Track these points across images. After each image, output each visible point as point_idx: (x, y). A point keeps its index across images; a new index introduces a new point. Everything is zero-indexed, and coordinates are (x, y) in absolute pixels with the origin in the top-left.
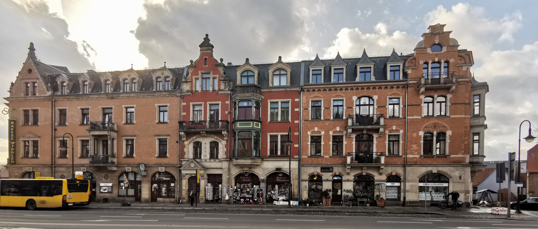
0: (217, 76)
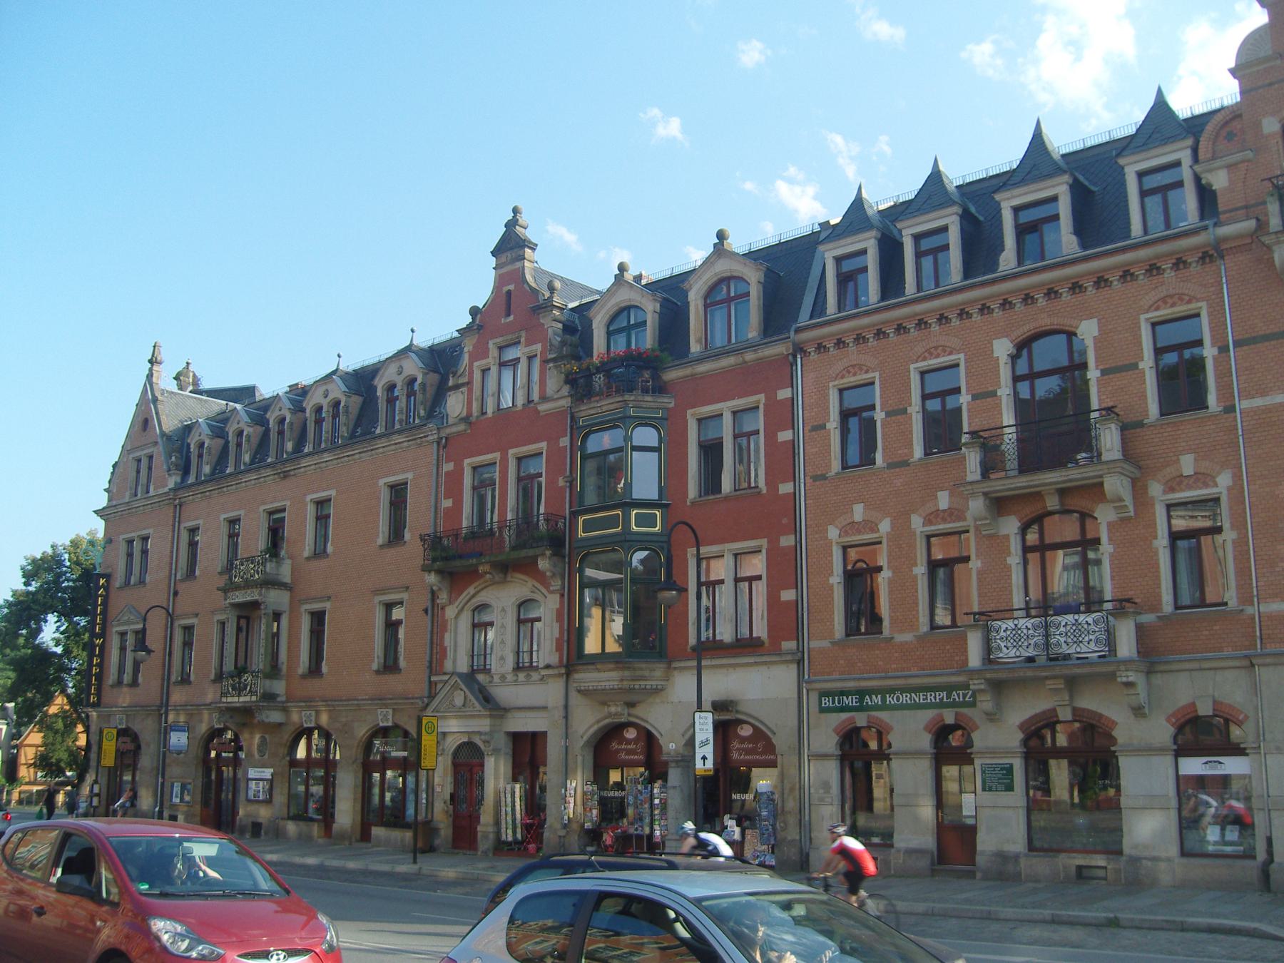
0: (538, 347)
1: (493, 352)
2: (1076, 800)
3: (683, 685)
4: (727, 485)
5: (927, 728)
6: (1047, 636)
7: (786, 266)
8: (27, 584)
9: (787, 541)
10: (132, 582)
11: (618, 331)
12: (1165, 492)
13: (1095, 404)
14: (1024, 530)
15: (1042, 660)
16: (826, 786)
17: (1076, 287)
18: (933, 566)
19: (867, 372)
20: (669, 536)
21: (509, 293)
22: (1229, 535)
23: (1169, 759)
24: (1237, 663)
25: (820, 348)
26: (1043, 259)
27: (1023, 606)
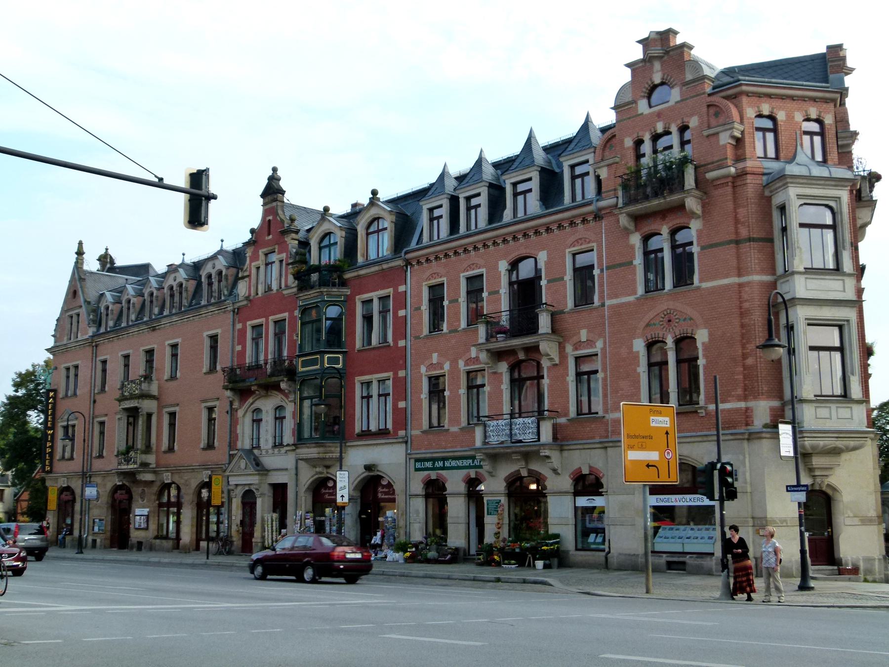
0: (284, 255)
1: (262, 257)
6: (511, 430)
8: (16, 391)
9: (401, 374)
10: (69, 394)
11: (325, 247)
12: (573, 350)
21: (269, 221)
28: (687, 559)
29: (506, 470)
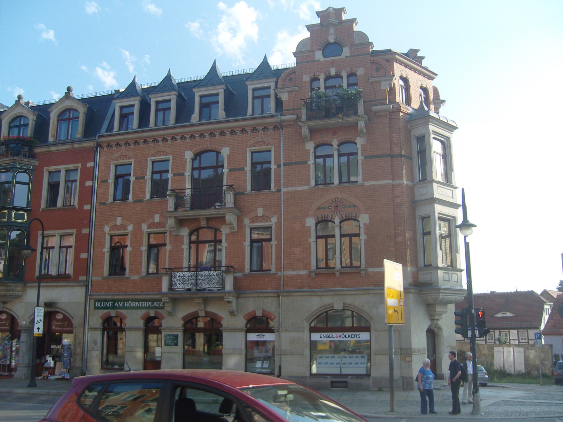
2: (206, 351)
3: (31, 295)
4: (60, 203)
5: (142, 318)
6: (196, 280)
7: (97, 107)
9: (85, 231)
11: (15, 127)
12: (250, 223)
13: (225, 183)
14: (191, 234)
15: (194, 290)
16: (95, 343)
17: (222, 133)
18: (150, 247)
19: (129, 159)
20: (30, 224)
22: (274, 242)
23: (243, 334)
24: (273, 295)
25: (109, 146)
26: (210, 119)
27: (187, 266)
28: (349, 379)
29: (184, 311)
